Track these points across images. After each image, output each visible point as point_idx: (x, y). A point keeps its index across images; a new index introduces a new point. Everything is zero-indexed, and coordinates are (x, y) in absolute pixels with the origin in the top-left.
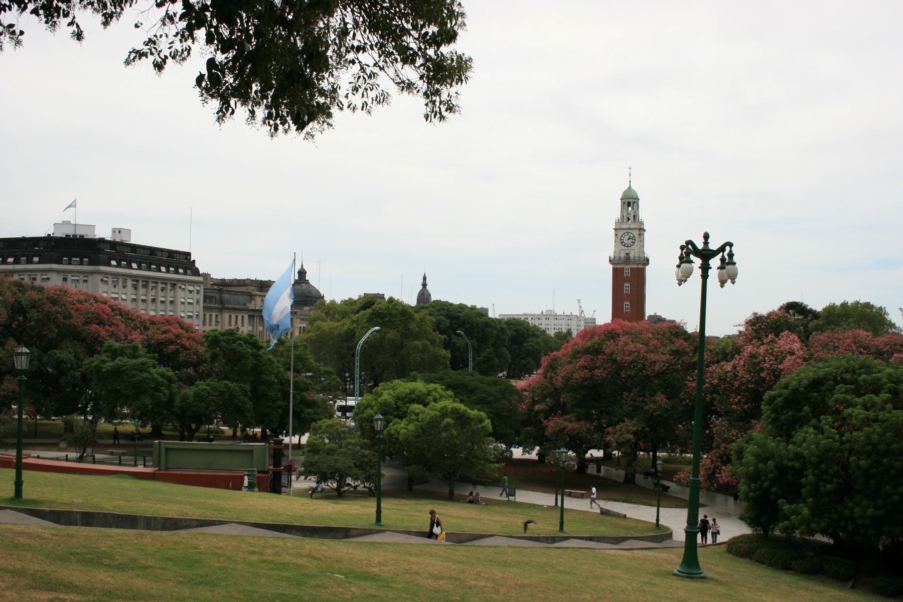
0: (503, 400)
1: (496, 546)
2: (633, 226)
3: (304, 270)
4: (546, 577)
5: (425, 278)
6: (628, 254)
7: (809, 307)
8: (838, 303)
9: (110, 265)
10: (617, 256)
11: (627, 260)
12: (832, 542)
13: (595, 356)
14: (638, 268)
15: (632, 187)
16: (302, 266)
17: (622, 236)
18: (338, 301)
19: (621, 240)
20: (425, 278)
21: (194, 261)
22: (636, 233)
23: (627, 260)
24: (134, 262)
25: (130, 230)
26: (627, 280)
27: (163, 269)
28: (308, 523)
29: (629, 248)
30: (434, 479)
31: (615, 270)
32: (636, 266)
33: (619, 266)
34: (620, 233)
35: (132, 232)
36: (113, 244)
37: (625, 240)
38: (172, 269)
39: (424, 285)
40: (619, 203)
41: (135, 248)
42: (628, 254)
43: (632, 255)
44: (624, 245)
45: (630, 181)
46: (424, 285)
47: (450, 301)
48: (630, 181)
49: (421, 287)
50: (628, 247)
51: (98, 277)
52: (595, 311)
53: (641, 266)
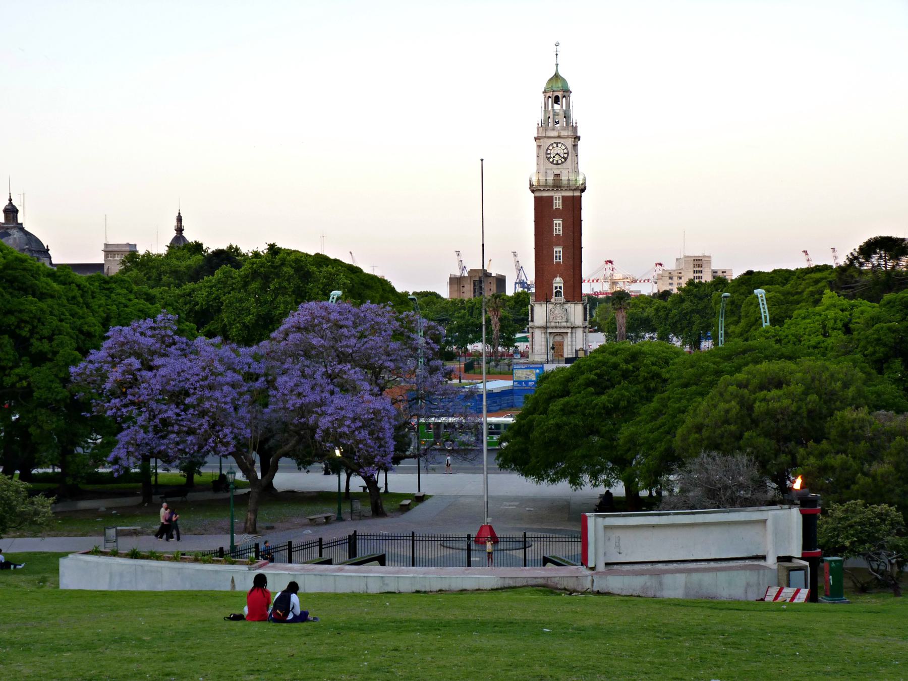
1: (462, 590)
3: (14, 207)
4: (664, 648)
5: (179, 219)
7: (141, 251)
10: (542, 179)
11: (557, 185)
12: (34, 472)
13: (122, 311)
14: (573, 196)
16: (10, 200)
17: (548, 149)
19: (547, 154)
20: (179, 219)
22: (569, 142)
23: (557, 185)
26: (558, 214)
29: (559, 166)
32: (570, 194)
34: (546, 143)
39: (10, 197)
40: (541, 98)
42: (557, 175)
43: (564, 178)
44: (552, 163)
45: (557, 65)
46: (10, 197)
48: (557, 65)
50: (557, 164)
52: (490, 260)
53: (577, 194)
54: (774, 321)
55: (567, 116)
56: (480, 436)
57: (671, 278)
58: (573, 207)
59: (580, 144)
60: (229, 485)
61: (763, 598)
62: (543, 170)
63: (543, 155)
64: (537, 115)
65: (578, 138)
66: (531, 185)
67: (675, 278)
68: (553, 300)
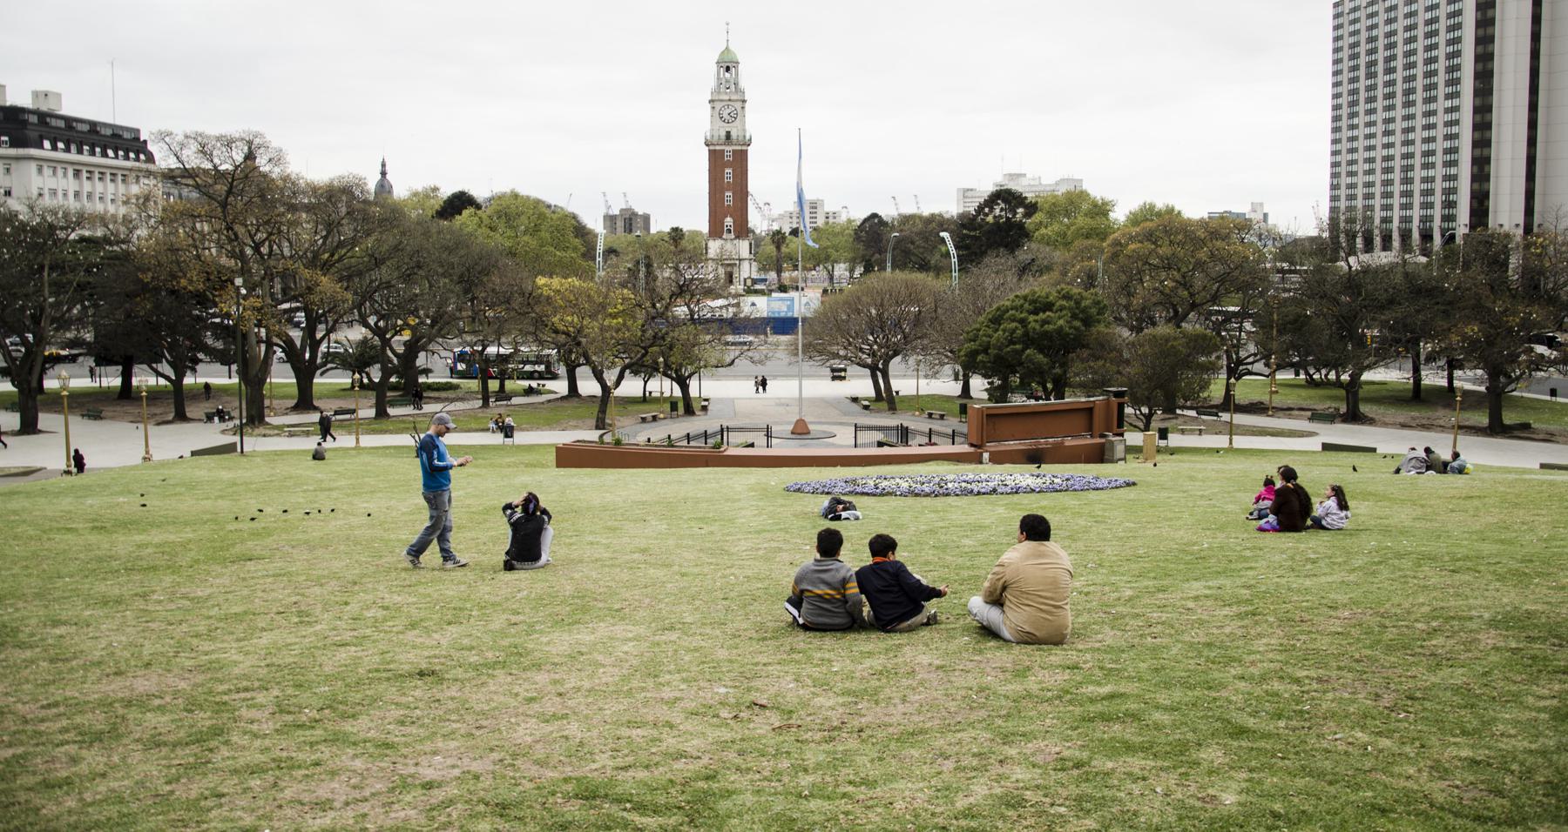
2: (734, 97)
5: (383, 165)
8: (508, 191)
9: (41, 147)
10: (716, 135)
15: (732, 47)
18: (401, 190)
20: (383, 165)
24: (47, 139)
27: (47, 144)
30: (151, 213)
32: (739, 148)
33: (718, 148)
34: (718, 105)
37: (725, 116)
39: (384, 174)
41: (69, 121)
43: (734, 135)
46: (384, 174)
47: (1234, 210)
49: (380, 176)
51: (33, 166)
53: (744, 148)
59: (747, 105)
64: (711, 83)
68: (724, 237)
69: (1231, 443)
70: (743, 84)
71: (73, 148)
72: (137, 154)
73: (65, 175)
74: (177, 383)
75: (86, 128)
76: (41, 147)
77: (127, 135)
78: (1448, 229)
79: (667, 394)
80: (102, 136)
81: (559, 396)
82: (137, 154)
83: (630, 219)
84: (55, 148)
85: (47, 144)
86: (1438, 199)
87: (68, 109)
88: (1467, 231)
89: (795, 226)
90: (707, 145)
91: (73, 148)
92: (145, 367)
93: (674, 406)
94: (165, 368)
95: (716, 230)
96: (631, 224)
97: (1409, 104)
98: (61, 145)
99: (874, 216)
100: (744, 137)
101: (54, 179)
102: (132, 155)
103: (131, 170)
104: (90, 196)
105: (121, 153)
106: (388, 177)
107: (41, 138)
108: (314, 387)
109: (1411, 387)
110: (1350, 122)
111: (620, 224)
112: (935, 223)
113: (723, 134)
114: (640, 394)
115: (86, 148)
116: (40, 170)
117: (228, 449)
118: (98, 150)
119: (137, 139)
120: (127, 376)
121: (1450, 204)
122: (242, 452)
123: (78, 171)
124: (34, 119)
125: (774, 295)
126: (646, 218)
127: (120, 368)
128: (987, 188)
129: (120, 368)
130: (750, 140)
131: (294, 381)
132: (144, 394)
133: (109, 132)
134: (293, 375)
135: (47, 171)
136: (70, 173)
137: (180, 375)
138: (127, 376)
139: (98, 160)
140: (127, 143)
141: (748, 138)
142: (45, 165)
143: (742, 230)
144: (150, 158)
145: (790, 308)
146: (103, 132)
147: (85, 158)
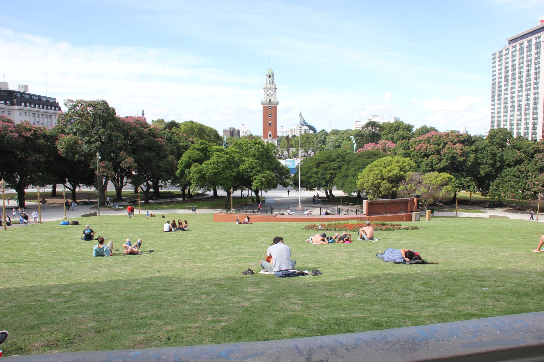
0: (338, 159)
2: (272, 87)
5: (143, 111)
6: (270, 100)
8: (478, 135)
9: (21, 105)
20: (143, 111)
21: (58, 103)
22: (274, 90)
24: (23, 102)
25: (8, 83)
27: (23, 104)
28: (516, 37)
29: (271, 97)
31: (264, 107)
32: (274, 105)
33: (266, 105)
35: (9, 84)
36: (21, 94)
38: (8, 102)
41: (31, 96)
53: (276, 105)
54: (359, 147)
55: (273, 82)
56: (34, 98)
57: (292, 131)
58: (275, 108)
59: (277, 90)
60: (103, 127)
61: (383, 253)
62: (266, 98)
63: (266, 93)
65: (276, 88)
66: (262, 102)
67: (293, 131)
68: (268, 138)
69: (456, 215)
70: (276, 82)
71: (32, 106)
72: (47, 106)
73: (29, 115)
74: (73, 191)
75: (37, 98)
76: (21, 105)
77: (52, 101)
78: (534, 138)
79: (250, 196)
80: (34, 99)
81: (210, 196)
82: (47, 106)
83: (233, 131)
84: (26, 105)
85: (23, 104)
86: (530, 126)
87: (31, 91)
88: (541, 138)
89: (293, 134)
90: (262, 104)
91: (32, 106)
92: (62, 185)
93: (253, 200)
94: (68, 184)
95: (265, 135)
96: (233, 133)
97: (520, 91)
98: (28, 104)
99: (323, 130)
100: (276, 101)
101: (25, 117)
102: (53, 108)
103: (53, 113)
104: (38, 122)
105: (49, 107)
106: (145, 116)
107: (21, 102)
108: (122, 192)
109: (453, 197)
110: (499, 98)
111: (229, 133)
112: (348, 133)
113: (268, 100)
114: (240, 196)
115: (45, 107)
116: (21, 114)
117: (95, 215)
118: (41, 106)
119: (55, 102)
120: (54, 188)
121: (534, 128)
122: (99, 215)
123: (34, 114)
124: (18, 95)
125: (287, 160)
126: (239, 131)
127: (52, 185)
128: (365, 122)
129: (52, 185)
130: (278, 102)
131: (115, 190)
132: (64, 194)
133: (45, 100)
134: (115, 188)
135: (23, 114)
136: (32, 115)
137: (75, 188)
138: (54, 188)
139: (45, 110)
140: (51, 104)
141: (277, 101)
142: (22, 112)
143: (275, 136)
144: (60, 109)
145: (293, 164)
146: (34, 98)
147: (37, 109)
